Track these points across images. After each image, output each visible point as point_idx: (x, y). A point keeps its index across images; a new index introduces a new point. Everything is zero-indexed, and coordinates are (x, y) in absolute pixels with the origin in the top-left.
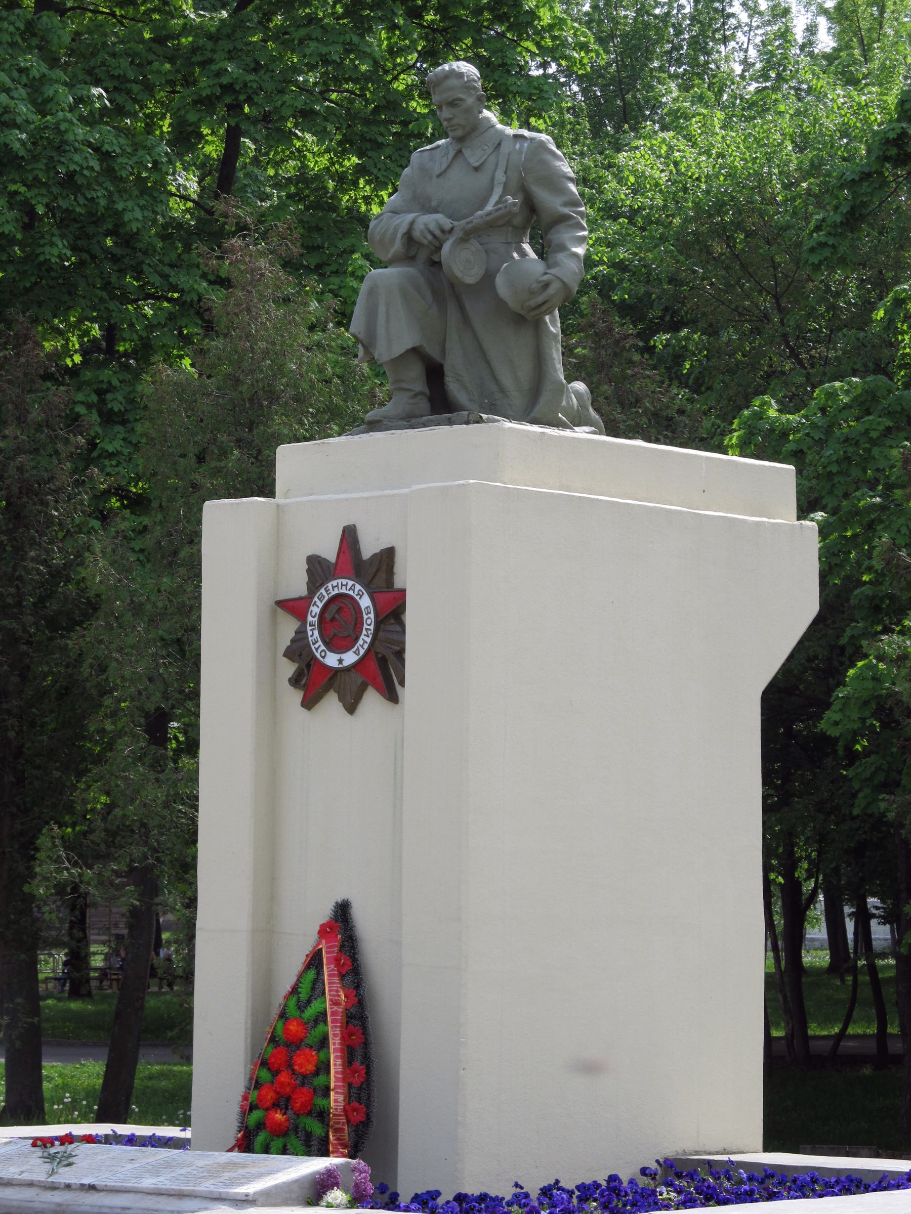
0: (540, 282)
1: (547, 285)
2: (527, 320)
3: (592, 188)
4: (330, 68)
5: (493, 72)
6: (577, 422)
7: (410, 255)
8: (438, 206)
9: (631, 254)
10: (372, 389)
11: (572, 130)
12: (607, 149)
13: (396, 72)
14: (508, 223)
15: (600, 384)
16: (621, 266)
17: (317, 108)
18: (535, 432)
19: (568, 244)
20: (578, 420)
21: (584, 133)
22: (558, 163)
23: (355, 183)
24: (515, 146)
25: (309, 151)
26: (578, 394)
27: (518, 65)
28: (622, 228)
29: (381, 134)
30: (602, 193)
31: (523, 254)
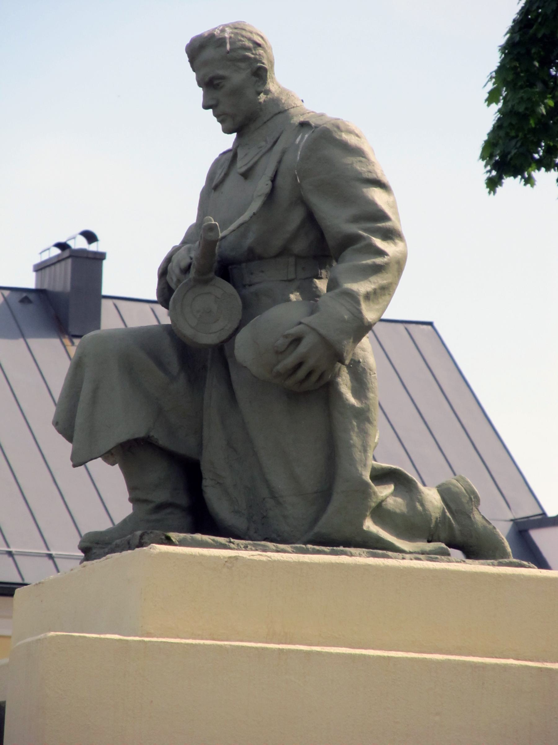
0: (286, 336)
1: (297, 340)
14: (284, 252)
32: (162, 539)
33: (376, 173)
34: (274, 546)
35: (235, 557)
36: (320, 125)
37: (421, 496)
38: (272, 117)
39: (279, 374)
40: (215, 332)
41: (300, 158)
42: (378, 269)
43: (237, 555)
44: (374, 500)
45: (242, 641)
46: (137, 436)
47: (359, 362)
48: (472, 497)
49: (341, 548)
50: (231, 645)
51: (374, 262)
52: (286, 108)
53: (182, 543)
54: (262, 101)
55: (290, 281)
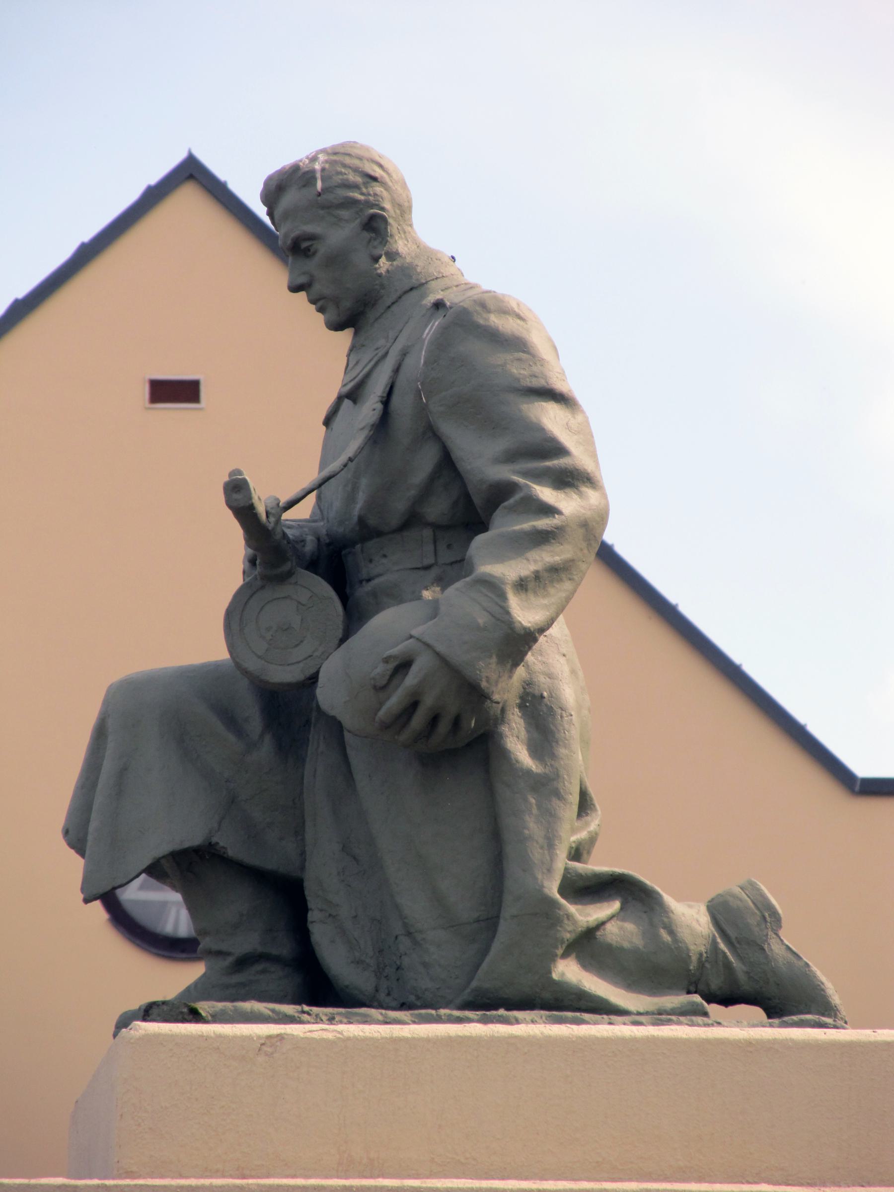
0: (386, 660)
1: (404, 666)
14: (412, 520)
32: (182, 1013)
33: (545, 378)
34: (381, 1014)
35: (278, 1035)
37: (668, 917)
38: (400, 297)
39: (386, 726)
40: (298, 662)
41: (425, 362)
42: (543, 538)
43: (283, 1031)
44: (569, 929)
45: (294, 1176)
46: (187, 845)
47: (542, 697)
48: (767, 915)
49: (502, 1012)
50: (258, 1185)
51: (534, 526)
52: (424, 281)
53: (218, 1018)
54: (382, 271)
55: (427, 568)
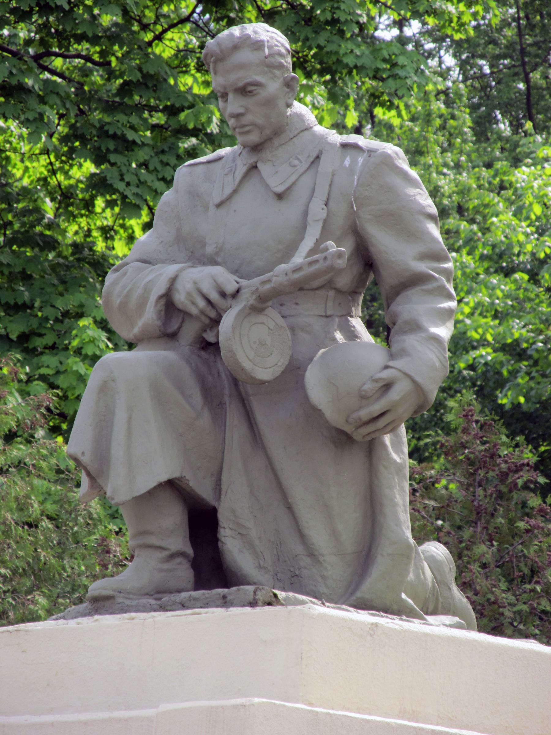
0: (377, 381)
1: (387, 386)
2: (354, 441)
3: (472, 221)
4: (51, 19)
5: (316, 32)
6: (431, 608)
7: (170, 330)
8: (217, 254)
9: (532, 331)
10: (104, 539)
11: (443, 127)
12: (499, 159)
13: (159, 28)
14: (329, 285)
15: (474, 543)
16: (515, 350)
17: (29, 82)
18: (363, 623)
19: (424, 321)
20: (433, 606)
21: (461, 134)
22: (412, 191)
23: (89, 205)
24: (343, 162)
25: (15, 150)
26: (433, 562)
27: (358, 23)
28: (518, 289)
29: (133, 128)
30: (488, 229)
31: (351, 335)
36: (378, 150)
